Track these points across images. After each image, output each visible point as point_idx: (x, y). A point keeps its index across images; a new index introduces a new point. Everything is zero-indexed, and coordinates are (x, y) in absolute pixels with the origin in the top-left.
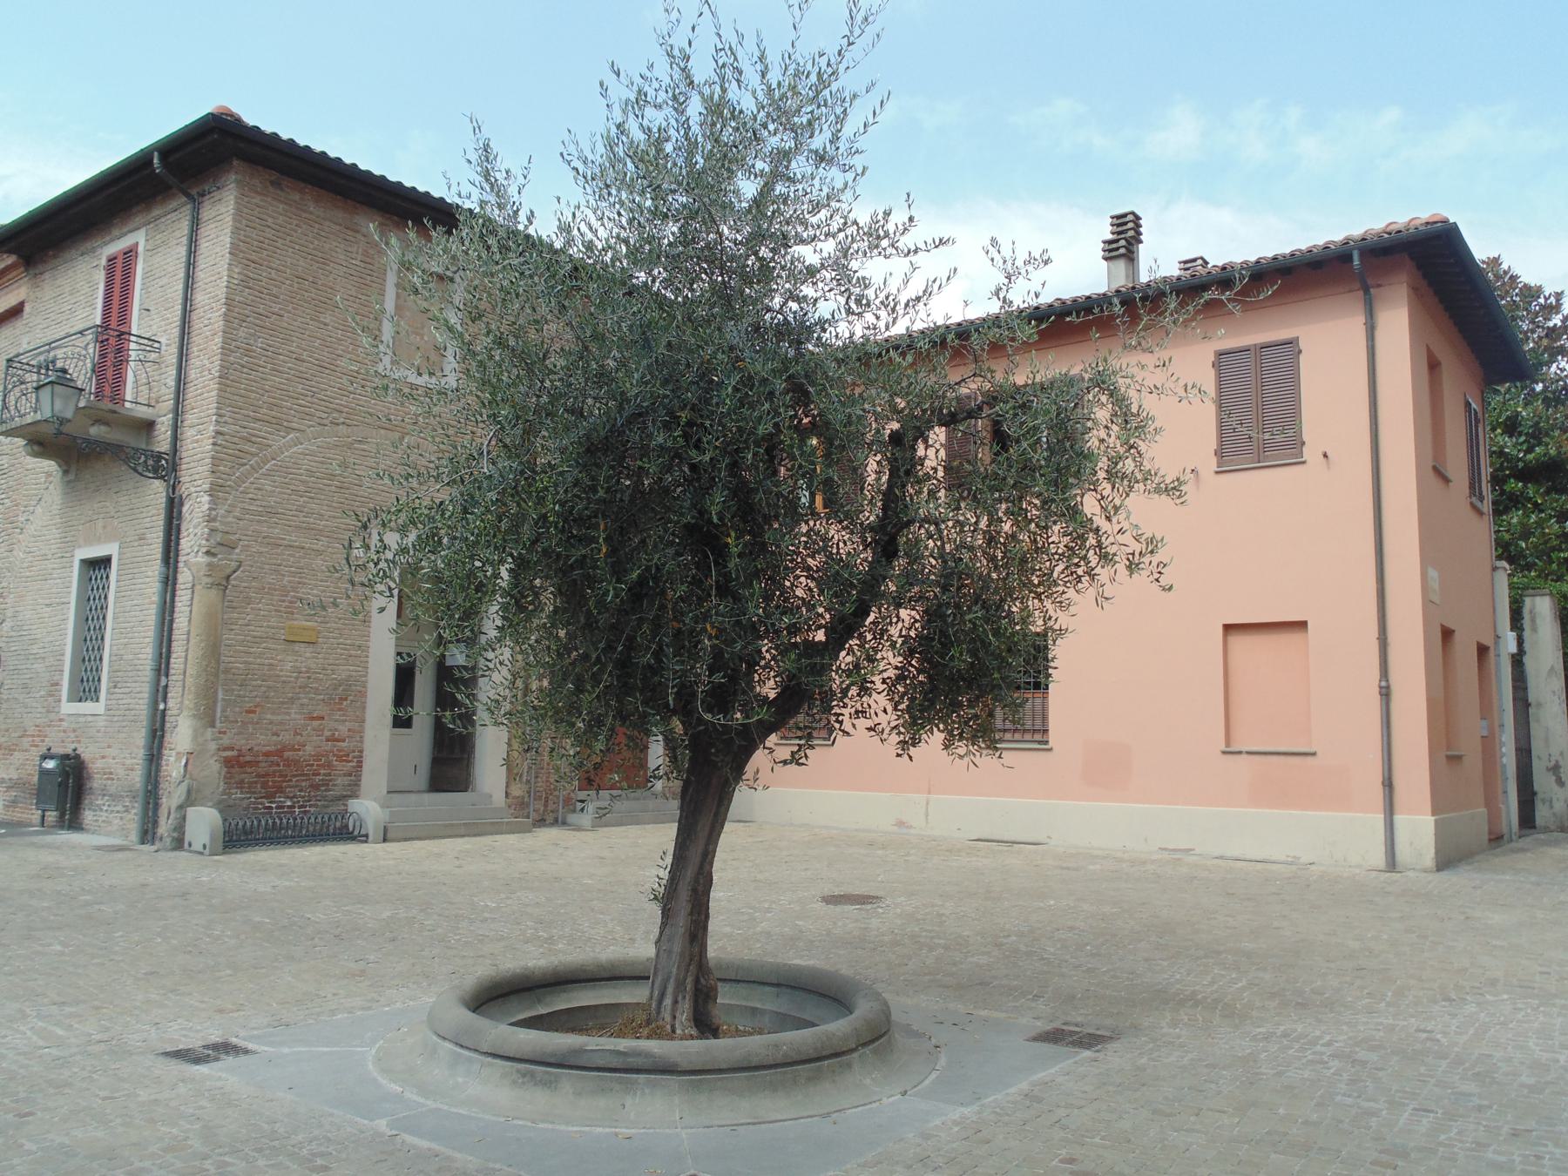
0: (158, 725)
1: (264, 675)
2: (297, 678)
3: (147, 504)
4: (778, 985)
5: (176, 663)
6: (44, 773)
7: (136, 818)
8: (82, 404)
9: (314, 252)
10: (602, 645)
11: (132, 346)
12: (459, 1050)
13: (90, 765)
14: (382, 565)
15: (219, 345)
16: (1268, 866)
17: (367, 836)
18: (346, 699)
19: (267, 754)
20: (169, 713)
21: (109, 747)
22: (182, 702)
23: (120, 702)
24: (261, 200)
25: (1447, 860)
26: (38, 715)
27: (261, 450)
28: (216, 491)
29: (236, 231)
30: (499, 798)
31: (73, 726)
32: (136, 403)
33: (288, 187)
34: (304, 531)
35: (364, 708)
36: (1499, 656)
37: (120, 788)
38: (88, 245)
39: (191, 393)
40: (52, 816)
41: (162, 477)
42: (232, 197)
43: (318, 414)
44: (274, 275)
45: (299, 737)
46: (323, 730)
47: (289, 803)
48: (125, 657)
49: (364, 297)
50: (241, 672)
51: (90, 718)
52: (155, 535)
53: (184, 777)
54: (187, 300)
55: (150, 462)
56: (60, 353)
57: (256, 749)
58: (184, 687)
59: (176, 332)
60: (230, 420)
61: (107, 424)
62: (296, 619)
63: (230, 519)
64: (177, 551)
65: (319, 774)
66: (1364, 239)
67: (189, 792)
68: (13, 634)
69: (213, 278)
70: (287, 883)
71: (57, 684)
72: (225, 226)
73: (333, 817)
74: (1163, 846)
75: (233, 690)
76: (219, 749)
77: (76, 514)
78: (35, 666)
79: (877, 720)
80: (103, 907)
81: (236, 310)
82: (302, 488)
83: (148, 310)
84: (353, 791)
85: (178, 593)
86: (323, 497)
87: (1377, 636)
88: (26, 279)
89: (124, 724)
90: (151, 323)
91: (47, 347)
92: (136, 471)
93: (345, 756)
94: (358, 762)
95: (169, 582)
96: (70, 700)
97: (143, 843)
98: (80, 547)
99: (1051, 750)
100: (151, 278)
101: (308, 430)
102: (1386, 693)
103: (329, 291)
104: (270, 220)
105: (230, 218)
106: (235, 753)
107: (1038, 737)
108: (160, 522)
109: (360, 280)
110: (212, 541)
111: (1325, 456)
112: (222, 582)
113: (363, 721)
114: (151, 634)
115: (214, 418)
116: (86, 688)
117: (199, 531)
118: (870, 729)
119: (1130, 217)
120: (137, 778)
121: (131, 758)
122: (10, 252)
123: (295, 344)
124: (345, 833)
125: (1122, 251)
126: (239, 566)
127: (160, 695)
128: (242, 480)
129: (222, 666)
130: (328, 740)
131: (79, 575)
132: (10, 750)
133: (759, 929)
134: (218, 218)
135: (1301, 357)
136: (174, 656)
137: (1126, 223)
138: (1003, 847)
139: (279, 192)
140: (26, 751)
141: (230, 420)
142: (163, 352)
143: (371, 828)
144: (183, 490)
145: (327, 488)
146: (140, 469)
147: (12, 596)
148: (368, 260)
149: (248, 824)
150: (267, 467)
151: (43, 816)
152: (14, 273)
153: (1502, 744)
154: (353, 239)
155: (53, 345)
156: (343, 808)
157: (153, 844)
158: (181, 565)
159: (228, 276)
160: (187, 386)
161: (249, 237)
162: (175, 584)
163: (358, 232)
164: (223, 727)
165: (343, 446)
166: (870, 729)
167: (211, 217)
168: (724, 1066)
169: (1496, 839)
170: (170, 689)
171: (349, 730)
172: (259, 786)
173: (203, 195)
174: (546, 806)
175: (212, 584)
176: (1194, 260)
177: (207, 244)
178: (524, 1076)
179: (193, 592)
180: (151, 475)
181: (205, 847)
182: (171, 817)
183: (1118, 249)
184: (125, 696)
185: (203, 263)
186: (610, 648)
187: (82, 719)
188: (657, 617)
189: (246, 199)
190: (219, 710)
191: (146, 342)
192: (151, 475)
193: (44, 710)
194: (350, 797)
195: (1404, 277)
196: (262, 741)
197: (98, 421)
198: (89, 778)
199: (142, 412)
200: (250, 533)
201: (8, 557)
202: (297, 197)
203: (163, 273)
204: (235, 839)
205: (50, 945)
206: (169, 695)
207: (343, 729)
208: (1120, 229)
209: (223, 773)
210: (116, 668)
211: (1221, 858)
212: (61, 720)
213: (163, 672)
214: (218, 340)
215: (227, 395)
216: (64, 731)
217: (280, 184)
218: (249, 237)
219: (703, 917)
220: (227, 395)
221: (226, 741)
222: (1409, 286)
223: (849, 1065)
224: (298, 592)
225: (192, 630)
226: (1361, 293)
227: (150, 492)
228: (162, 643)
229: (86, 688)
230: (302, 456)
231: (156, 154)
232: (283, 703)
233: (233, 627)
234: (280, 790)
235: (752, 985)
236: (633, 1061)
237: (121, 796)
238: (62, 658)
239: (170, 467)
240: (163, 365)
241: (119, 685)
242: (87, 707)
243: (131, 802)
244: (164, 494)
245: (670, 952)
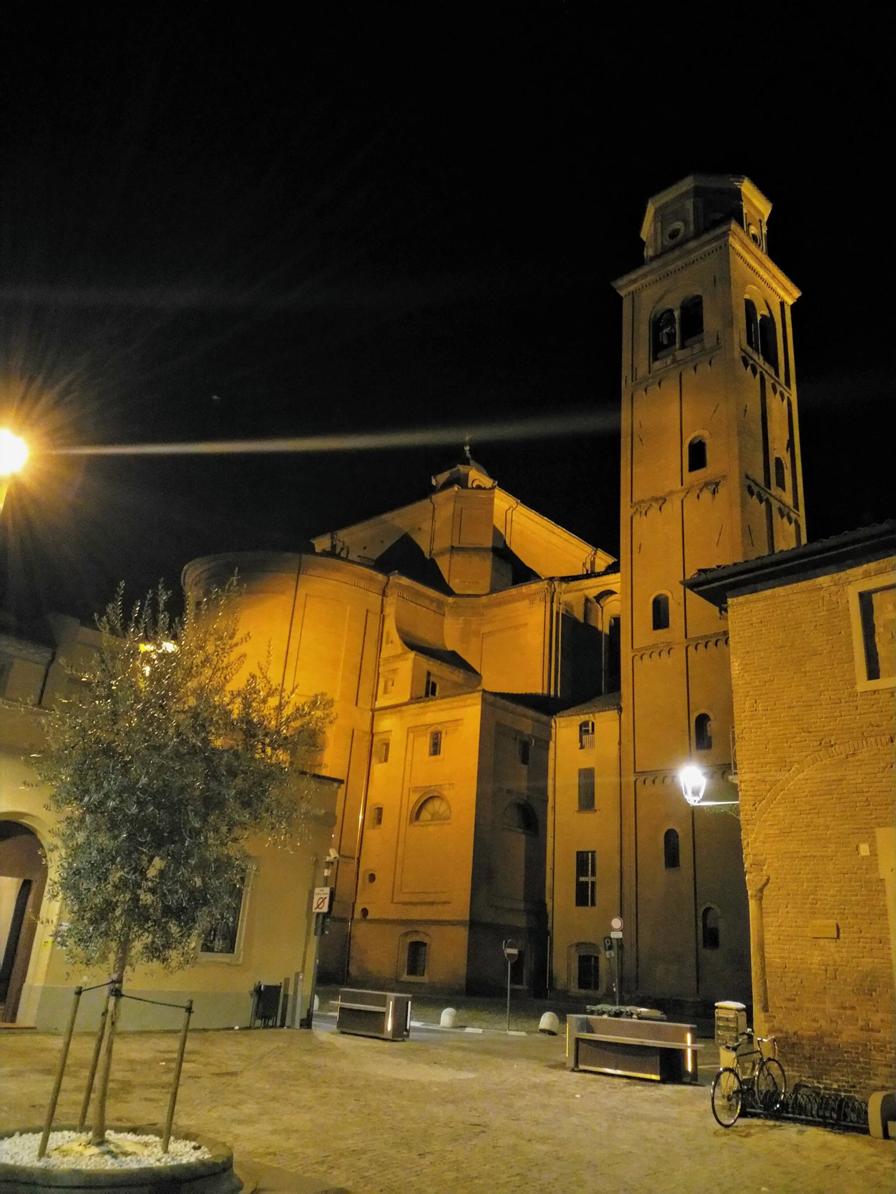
47: (835, 1086)
106: (784, 1035)
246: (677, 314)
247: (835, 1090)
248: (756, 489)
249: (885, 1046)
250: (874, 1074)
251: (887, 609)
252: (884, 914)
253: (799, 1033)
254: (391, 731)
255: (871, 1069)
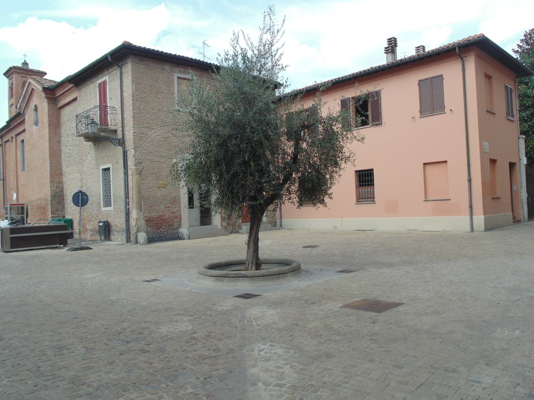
0: (127, 212)
1: (153, 197)
2: (162, 197)
3: (118, 153)
4: (278, 263)
5: (130, 195)
6: (100, 226)
7: (125, 237)
8: (98, 128)
9: (154, 78)
10: (226, 188)
11: (108, 110)
12: (204, 276)
13: (111, 224)
14: (178, 174)
15: (132, 108)
16: (434, 233)
17: (184, 238)
18: (175, 202)
19: (156, 218)
20: (130, 208)
21: (116, 219)
22: (133, 206)
23: (117, 206)
24: (139, 65)
25: (489, 227)
26: (96, 211)
27: (146, 136)
28: (135, 148)
29: (132, 75)
30: (219, 226)
31: (105, 214)
32: (112, 125)
33: (145, 60)
34: (159, 157)
35: (180, 204)
36: (520, 165)
37: (120, 229)
38: (93, 80)
39: (126, 122)
40: (103, 237)
41: (121, 145)
42: (130, 66)
43: (160, 124)
44: (144, 86)
45: (164, 213)
46: (170, 210)
47: (163, 231)
48: (117, 194)
49: (168, 89)
50: (147, 196)
51: (109, 211)
52: (121, 161)
53: (136, 225)
54: (122, 96)
55: (118, 142)
56: (90, 113)
57: (153, 217)
58: (133, 201)
59: (120, 104)
60: (137, 129)
61: (105, 132)
62: (160, 181)
63: (140, 156)
64: (127, 165)
65: (170, 222)
66: (459, 43)
67: (137, 229)
68: (86, 190)
69: (128, 89)
70: (165, 250)
71: (100, 203)
72: (129, 74)
73: (175, 233)
74: (408, 229)
75: (146, 201)
76: (144, 217)
77: (99, 156)
78: (93, 198)
79: (293, 200)
80: (122, 257)
81: (135, 97)
82: (158, 145)
83: (112, 99)
84: (180, 226)
85: (129, 176)
86: (163, 147)
87: (467, 164)
88: (76, 90)
89: (119, 212)
90: (112, 102)
91: (87, 112)
92: (114, 144)
93: (176, 217)
94: (180, 219)
95: (126, 174)
96: (103, 207)
97: (127, 243)
98: (101, 165)
99: (376, 203)
100: (111, 89)
101: (158, 129)
102: (470, 181)
103: (159, 88)
104: (141, 71)
105: (130, 72)
106: (148, 218)
107: (372, 200)
108: (122, 158)
109: (167, 84)
110: (136, 162)
111: (451, 110)
112: (140, 173)
113: (180, 207)
114: (123, 188)
115: (133, 128)
116: (108, 203)
117: (132, 159)
118: (291, 202)
119: (393, 39)
120: (124, 226)
121: (122, 221)
122: (71, 84)
123: (151, 105)
124: (178, 237)
125: (390, 50)
126: (144, 168)
127: (127, 204)
128: (142, 144)
129: (142, 195)
130: (171, 213)
131: (102, 172)
132: (89, 221)
133: (283, 254)
134: (127, 72)
135: (444, 80)
136: (129, 193)
137: (392, 41)
138: (362, 232)
139: (143, 62)
140: (94, 221)
141: (137, 129)
142: (117, 111)
143: (185, 236)
144: (127, 148)
145: (164, 144)
146: (115, 143)
147: (84, 180)
148: (169, 78)
149: (153, 236)
150: (148, 140)
151: (101, 238)
152: (73, 89)
153: (521, 193)
154: (164, 72)
155: (88, 111)
156: (177, 231)
157: (130, 243)
158: (128, 169)
159: (132, 88)
160: (124, 120)
161: (136, 76)
162: (128, 174)
163: (165, 70)
164: (144, 211)
165: (168, 132)
166: (291, 202)
167: (125, 71)
168: (258, 276)
169: (516, 221)
170: (129, 202)
171: (177, 210)
172: (155, 226)
173: (123, 65)
174: (233, 228)
175: (137, 174)
176: (420, 47)
177: (125, 79)
178: (217, 280)
179: (133, 176)
180: (118, 145)
181: (143, 243)
182: (134, 235)
183: (389, 50)
184: (118, 205)
185: (125, 85)
186: (228, 189)
187: (107, 212)
188: (238, 181)
189: (134, 66)
190: (143, 207)
191: (112, 108)
192: (118, 145)
193: (97, 210)
194: (179, 228)
195: (473, 53)
196: (155, 215)
197: (103, 131)
198: (111, 227)
199: (113, 128)
200: (145, 159)
201: (82, 169)
202: (147, 63)
203: (114, 88)
204: (151, 240)
205: (113, 264)
206: (129, 204)
207: (175, 210)
208: (390, 43)
209: (146, 224)
210: (115, 198)
211: (424, 231)
212: (102, 212)
213: (127, 198)
214: (131, 106)
215: (135, 122)
216: (103, 215)
217: (142, 60)
218: (136, 76)
219: (256, 247)
220: (135, 122)
221: (145, 215)
222: (475, 55)
223: (287, 276)
224: (159, 174)
225: (133, 186)
226: (460, 59)
227: (118, 149)
228: (126, 190)
229: (108, 203)
230: (157, 136)
231: (109, 55)
232: (158, 204)
233: (144, 185)
234: (160, 227)
235: (273, 264)
236: (238, 275)
237: (120, 231)
238: (100, 196)
239: (123, 142)
240: (117, 114)
241: (116, 202)
242: (108, 208)
243: (123, 232)
244: (122, 150)
245: (249, 255)
251: (183, 85)
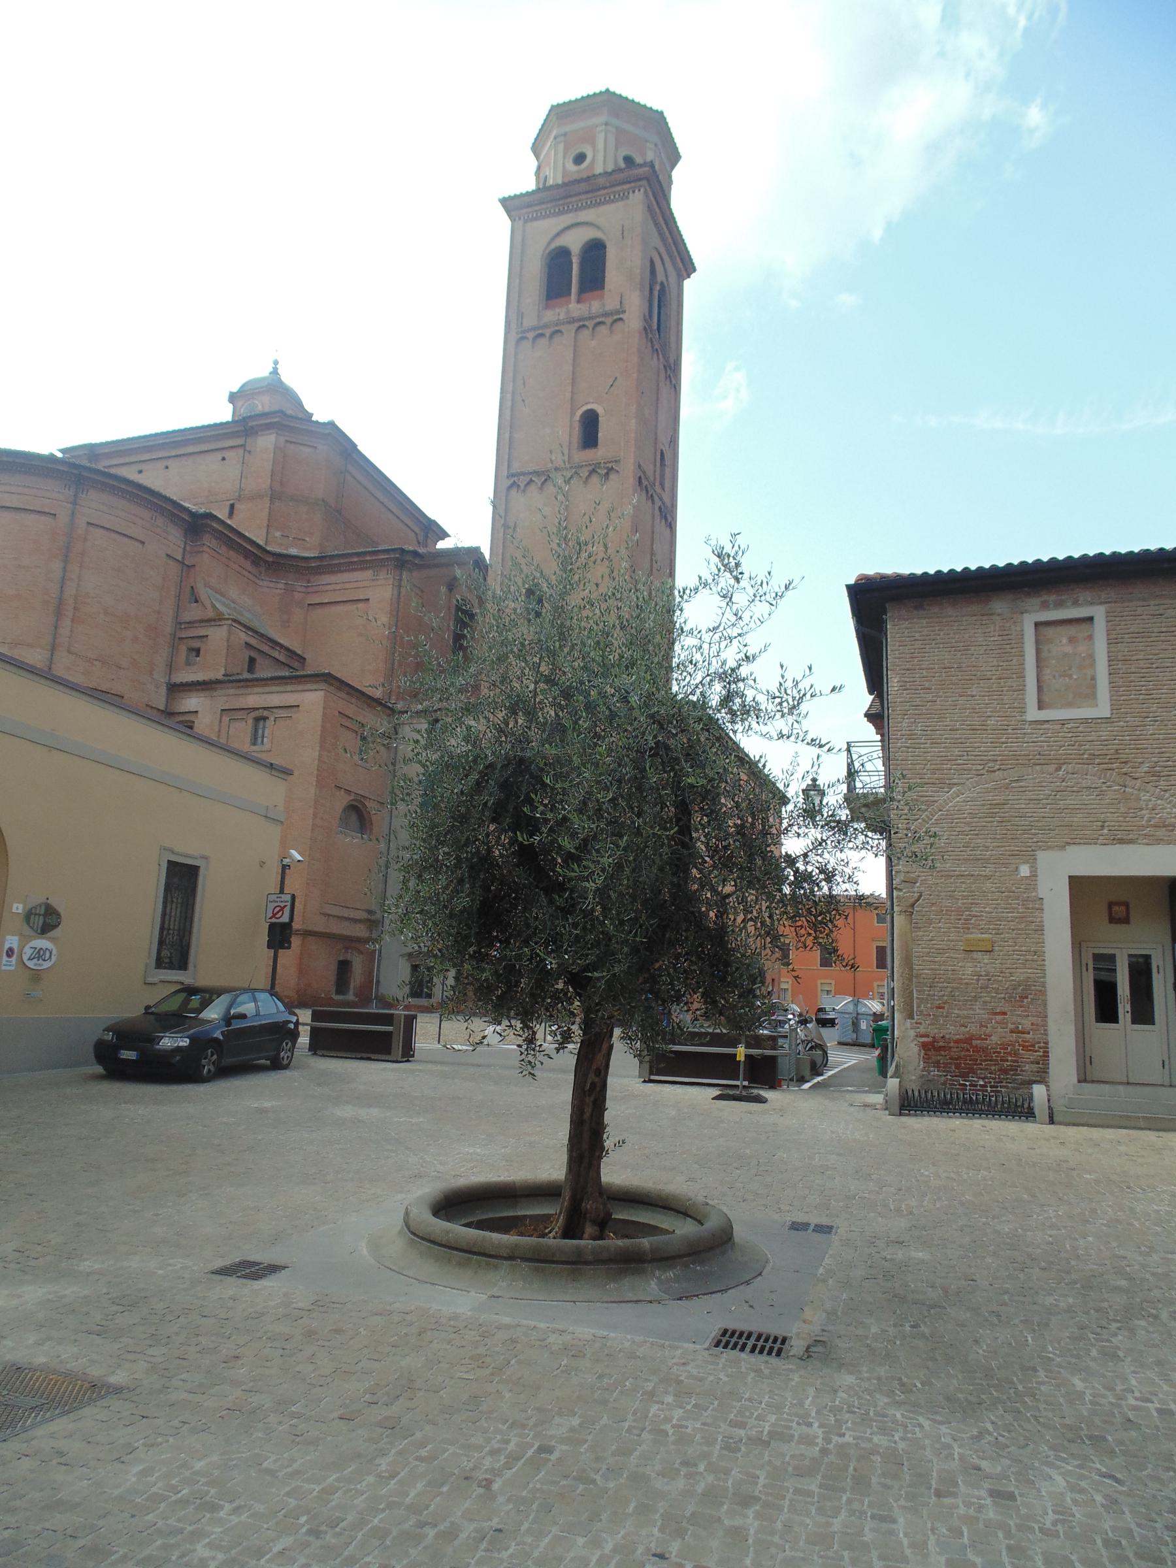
106: (930, 1039)
246: (575, 261)
247: (981, 1086)
248: (645, 482)
249: (1033, 1046)
250: (1022, 1071)
252: (1040, 929)
253: (947, 1036)
254: (197, 712)
255: (1019, 1066)
